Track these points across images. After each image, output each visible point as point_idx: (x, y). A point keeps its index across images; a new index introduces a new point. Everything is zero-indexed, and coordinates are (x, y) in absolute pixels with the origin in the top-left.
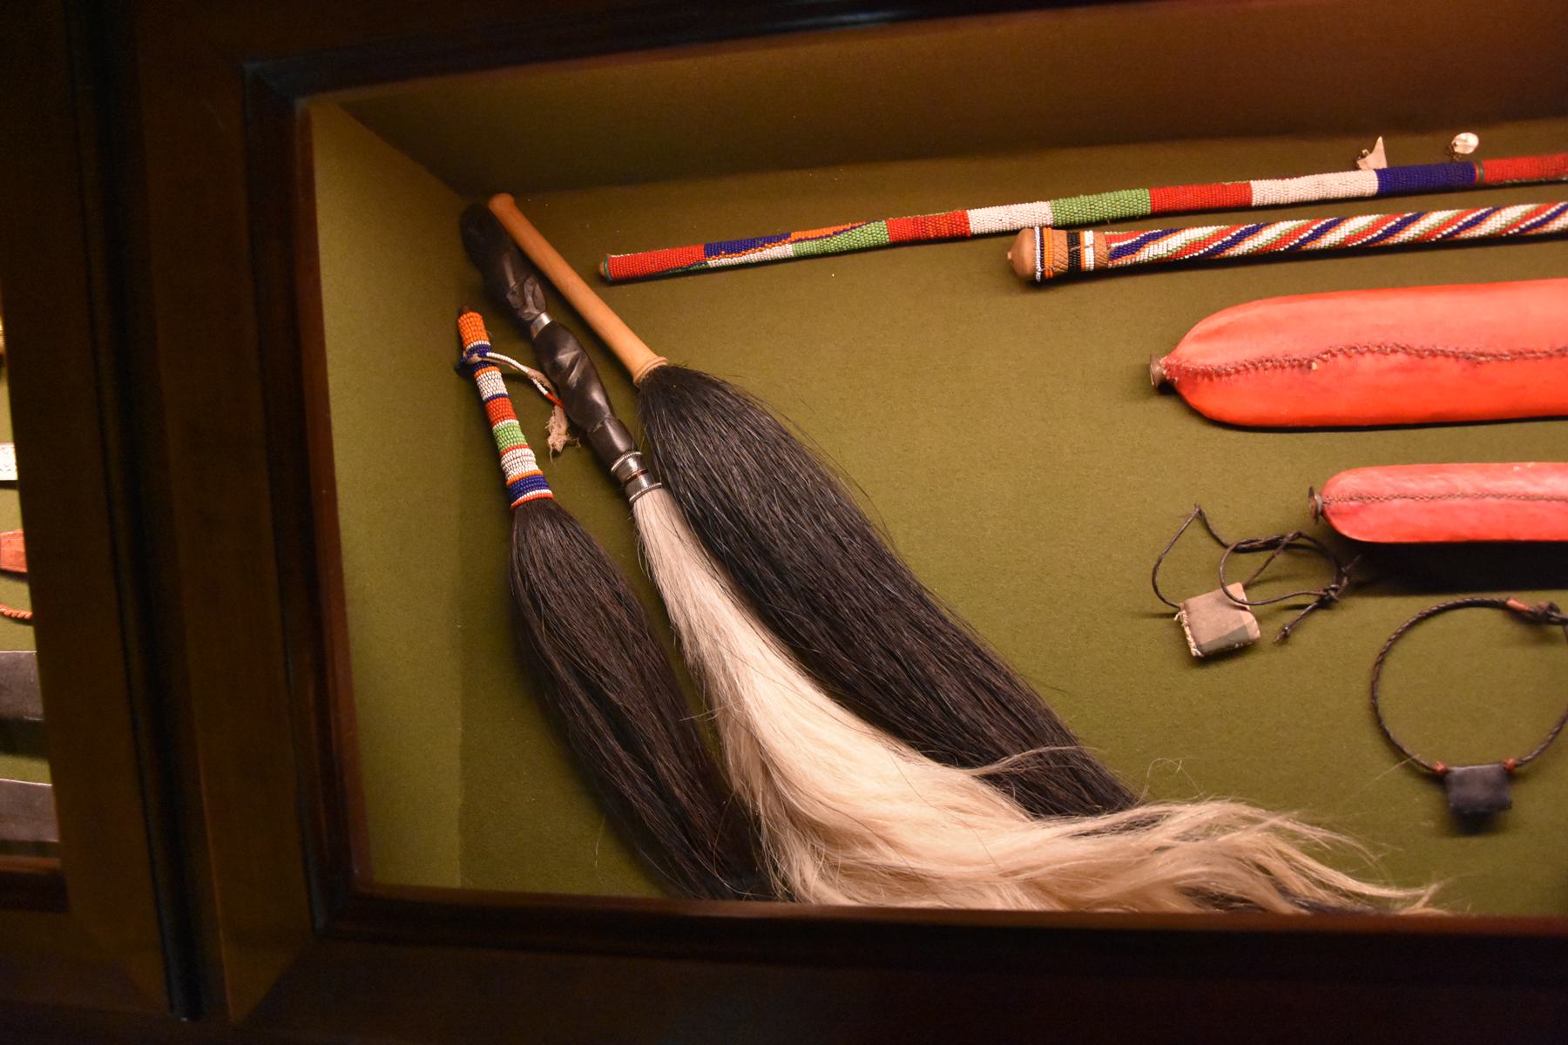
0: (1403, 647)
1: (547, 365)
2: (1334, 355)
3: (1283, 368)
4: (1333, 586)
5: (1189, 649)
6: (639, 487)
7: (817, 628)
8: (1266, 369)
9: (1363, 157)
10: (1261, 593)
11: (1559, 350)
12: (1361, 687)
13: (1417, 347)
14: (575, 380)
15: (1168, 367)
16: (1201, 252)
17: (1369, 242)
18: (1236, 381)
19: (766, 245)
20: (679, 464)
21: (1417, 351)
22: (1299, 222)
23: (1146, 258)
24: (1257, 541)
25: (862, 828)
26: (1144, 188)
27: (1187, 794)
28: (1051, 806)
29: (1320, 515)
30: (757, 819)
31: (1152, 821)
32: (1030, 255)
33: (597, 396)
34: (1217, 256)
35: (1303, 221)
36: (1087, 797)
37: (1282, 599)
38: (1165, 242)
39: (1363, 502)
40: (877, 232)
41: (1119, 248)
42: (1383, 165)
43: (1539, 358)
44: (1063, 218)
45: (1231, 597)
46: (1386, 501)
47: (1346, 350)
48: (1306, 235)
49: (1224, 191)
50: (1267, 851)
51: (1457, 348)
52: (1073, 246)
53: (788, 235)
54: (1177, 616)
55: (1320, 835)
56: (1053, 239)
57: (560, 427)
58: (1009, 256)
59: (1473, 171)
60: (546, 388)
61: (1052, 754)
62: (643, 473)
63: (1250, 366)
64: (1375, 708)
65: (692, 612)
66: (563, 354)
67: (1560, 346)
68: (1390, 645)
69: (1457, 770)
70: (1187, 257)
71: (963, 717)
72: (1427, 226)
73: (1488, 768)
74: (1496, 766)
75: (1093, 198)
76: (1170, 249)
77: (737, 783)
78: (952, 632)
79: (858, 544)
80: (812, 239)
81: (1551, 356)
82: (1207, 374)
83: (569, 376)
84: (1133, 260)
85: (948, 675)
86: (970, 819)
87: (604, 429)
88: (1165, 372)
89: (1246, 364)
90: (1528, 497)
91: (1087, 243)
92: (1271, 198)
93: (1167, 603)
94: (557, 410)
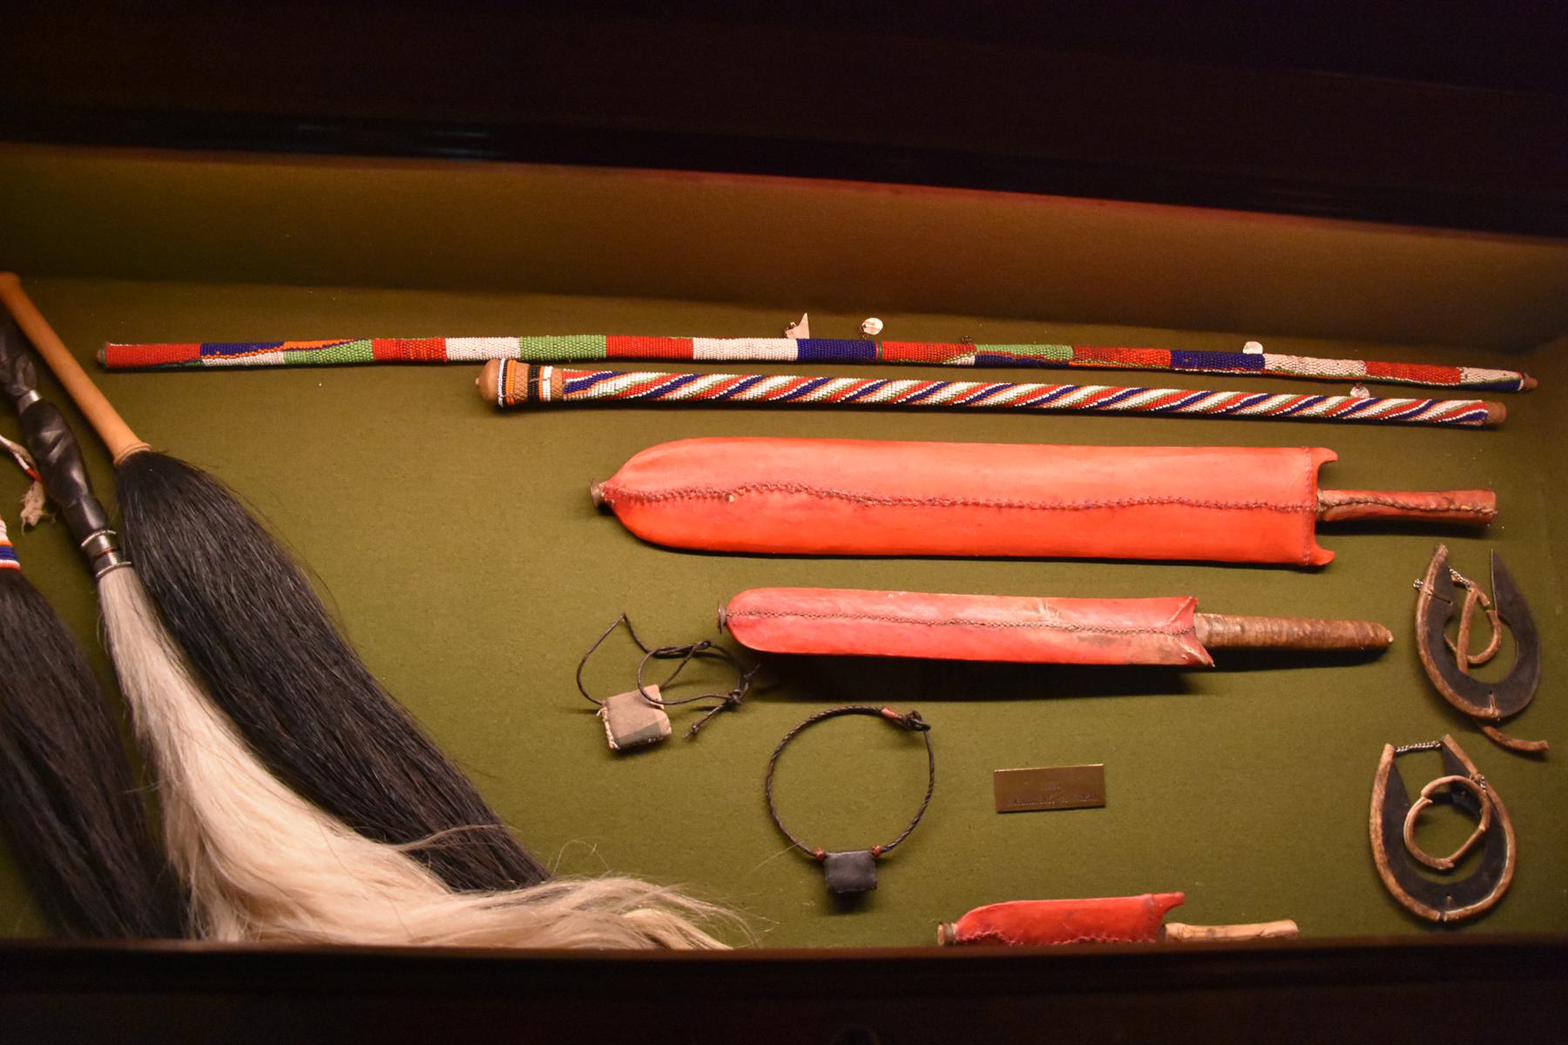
0: (794, 747)
1: (30, 441)
2: (748, 491)
3: (705, 498)
4: (736, 690)
5: (608, 742)
6: (107, 563)
7: (264, 707)
8: (690, 498)
9: (791, 328)
10: (673, 695)
11: (930, 500)
12: (758, 782)
13: (817, 489)
14: (56, 457)
15: (606, 490)
16: (644, 393)
17: (786, 398)
18: (664, 506)
19: (259, 350)
20: (145, 543)
21: (817, 492)
22: (730, 376)
23: (596, 394)
24: (674, 648)
25: (283, 895)
26: (602, 335)
27: (595, 871)
28: (469, 881)
29: (724, 625)
30: (189, 891)
31: (558, 893)
32: (494, 381)
33: (77, 475)
34: (658, 399)
35: (733, 376)
36: (503, 872)
37: (691, 700)
38: (614, 382)
39: (761, 617)
40: (362, 349)
41: (573, 383)
42: (807, 336)
43: (915, 506)
44: (529, 354)
45: (646, 696)
46: (781, 617)
47: (758, 486)
48: (733, 387)
49: (670, 343)
50: (667, 927)
51: (849, 492)
52: (533, 377)
53: (282, 344)
54: (599, 712)
55: (695, 905)
56: (515, 370)
57: (36, 501)
58: (477, 382)
59: (874, 349)
60: (28, 463)
61: (474, 831)
62: (113, 551)
63: (676, 495)
64: (768, 800)
65: (145, 687)
66: (48, 431)
67: (931, 497)
68: (784, 745)
69: (834, 855)
70: (632, 397)
71: (393, 796)
72: (833, 389)
73: (861, 854)
74: (866, 852)
75: (557, 339)
76: (617, 388)
77: (173, 855)
78: (393, 717)
79: (311, 631)
80: (303, 349)
81: (923, 504)
82: (639, 499)
83: (52, 450)
84: (585, 395)
85: (385, 757)
86: (392, 891)
87: (79, 505)
88: (603, 494)
89: (673, 492)
90: (897, 620)
91: (545, 377)
92: (708, 355)
93: (590, 699)
94: (37, 486)
